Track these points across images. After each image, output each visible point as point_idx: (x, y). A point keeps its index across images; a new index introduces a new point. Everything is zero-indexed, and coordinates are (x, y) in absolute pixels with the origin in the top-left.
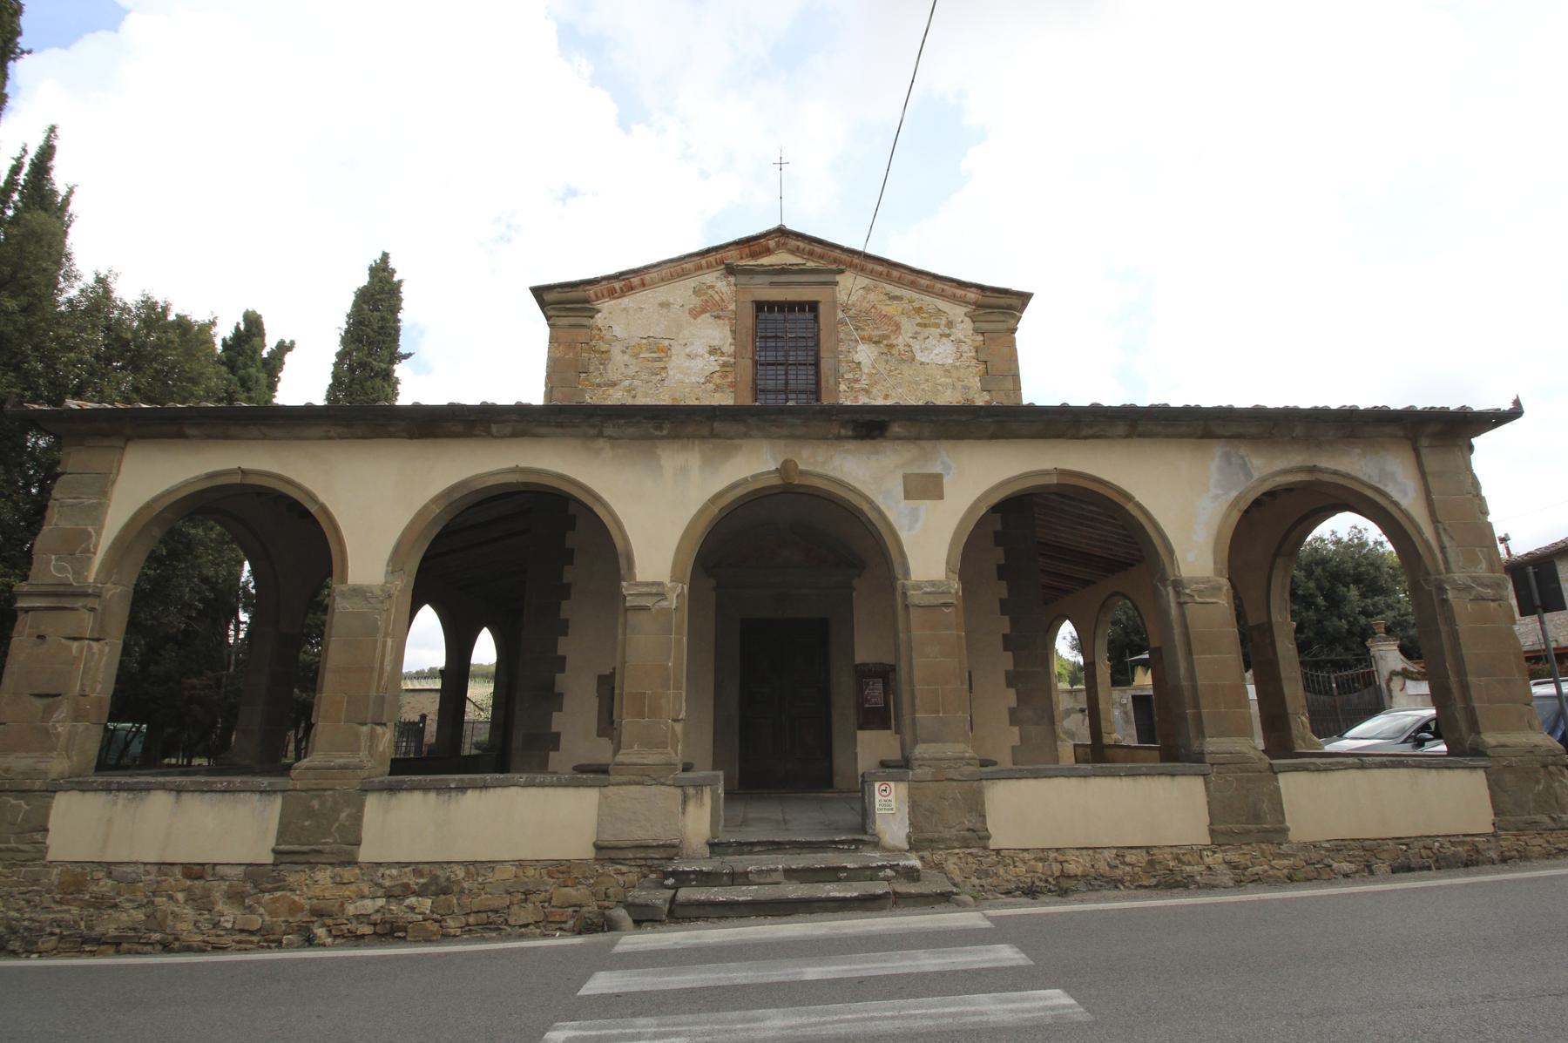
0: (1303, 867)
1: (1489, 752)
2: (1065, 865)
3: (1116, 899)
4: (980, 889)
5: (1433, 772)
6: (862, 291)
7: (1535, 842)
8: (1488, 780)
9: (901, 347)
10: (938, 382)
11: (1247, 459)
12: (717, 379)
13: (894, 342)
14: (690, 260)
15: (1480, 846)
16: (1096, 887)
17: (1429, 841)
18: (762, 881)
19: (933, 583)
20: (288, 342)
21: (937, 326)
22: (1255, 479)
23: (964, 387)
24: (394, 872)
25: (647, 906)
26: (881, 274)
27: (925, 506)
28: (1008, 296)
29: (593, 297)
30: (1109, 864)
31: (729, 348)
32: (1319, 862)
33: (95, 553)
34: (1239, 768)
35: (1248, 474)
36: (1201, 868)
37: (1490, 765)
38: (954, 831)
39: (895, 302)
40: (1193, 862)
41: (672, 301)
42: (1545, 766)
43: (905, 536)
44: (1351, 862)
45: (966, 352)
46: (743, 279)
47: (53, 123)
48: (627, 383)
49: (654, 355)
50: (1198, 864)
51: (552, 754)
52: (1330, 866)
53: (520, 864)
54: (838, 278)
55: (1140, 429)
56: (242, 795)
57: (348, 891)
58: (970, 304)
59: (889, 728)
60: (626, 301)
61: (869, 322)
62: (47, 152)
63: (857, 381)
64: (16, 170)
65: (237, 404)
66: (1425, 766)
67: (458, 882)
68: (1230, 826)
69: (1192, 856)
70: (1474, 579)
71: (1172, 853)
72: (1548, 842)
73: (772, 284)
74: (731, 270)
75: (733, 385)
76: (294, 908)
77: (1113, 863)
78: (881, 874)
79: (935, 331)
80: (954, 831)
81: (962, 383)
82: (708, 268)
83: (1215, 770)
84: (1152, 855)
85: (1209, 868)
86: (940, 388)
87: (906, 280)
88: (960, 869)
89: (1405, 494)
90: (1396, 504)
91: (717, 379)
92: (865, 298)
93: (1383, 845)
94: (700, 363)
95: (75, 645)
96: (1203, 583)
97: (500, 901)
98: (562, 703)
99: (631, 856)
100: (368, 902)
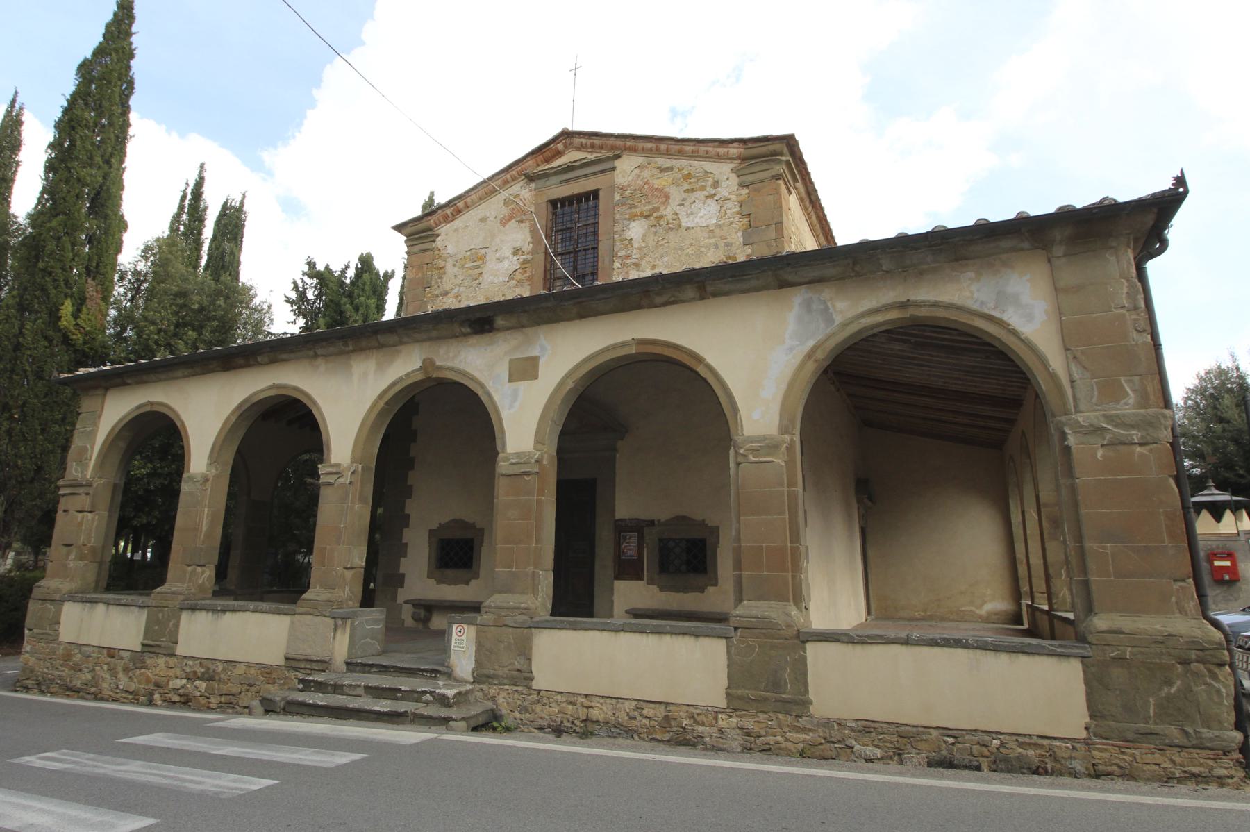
0: (821, 744)
1: (1091, 638)
2: (591, 710)
3: (627, 748)
4: (520, 722)
5: (1004, 657)
6: (637, 171)
7: (1149, 758)
8: (1084, 672)
9: (669, 217)
10: (702, 244)
11: (829, 304)
12: (518, 276)
13: (663, 213)
14: (497, 177)
15: (1060, 754)
16: (615, 735)
17: (986, 737)
18: (350, 693)
19: (762, 439)
20: (390, 271)
21: (703, 188)
22: (836, 324)
23: (727, 245)
24: (191, 663)
25: (271, 700)
26: (651, 150)
27: (523, 385)
28: (770, 143)
29: (434, 225)
30: (628, 714)
31: (527, 247)
32: (839, 742)
33: (90, 460)
34: (764, 634)
35: (829, 320)
36: (714, 730)
37: (1090, 654)
38: (506, 670)
39: (666, 174)
40: (706, 724)
41: (488, 215)
42: (1185, 662)
43: (505, 414)
44: (877, 747)
45: (730, 209)
46: (541, 183)
47: (203, 161)
48: (455, 291)
49: (475, 264)
50: (711, 725)
51: (400, 590)
52: (852, 748)
53: (248, 665)
54: (617, 163)
55: (709, 289)
56: (132, 608)
57: (171, 673)
58: (733, 159)
59: (640, 578)
60: (458, 223)
61: (642, 198)
62: (200, 183)
63: (628, 257)
64: (183, 198)
65: (199, 351)
66: (991, 648)
67: (218, 674)
68: (747, 691)
69: (707, 717)
70: (1109, 419)
71: (687, 712)
72: (1173, 762)
73: (562, 182)
74: (531, 178)
75: (529, 279)
76: (148, 681)
77: (632, 714)
78: (424, 698)
79: (701, 194)
80: (506, 670)
81: (725, 241)
82: (513, 180)
83: (739, 634)
84: (669, 711)
85: (721, 731)
86: (703, 249)
87: (673, 151)
88: (508, 703)
89: (1030, 318)
90: (1014, 333)
91: (518, 276)
92: (639, 176)
93: (923, 733)
94: (506, 264)
95: (80, 515)
96: (758, 442)
97: (235, 689)
98: (406, 551)
99: (303, 666)
100: (178, 681)
